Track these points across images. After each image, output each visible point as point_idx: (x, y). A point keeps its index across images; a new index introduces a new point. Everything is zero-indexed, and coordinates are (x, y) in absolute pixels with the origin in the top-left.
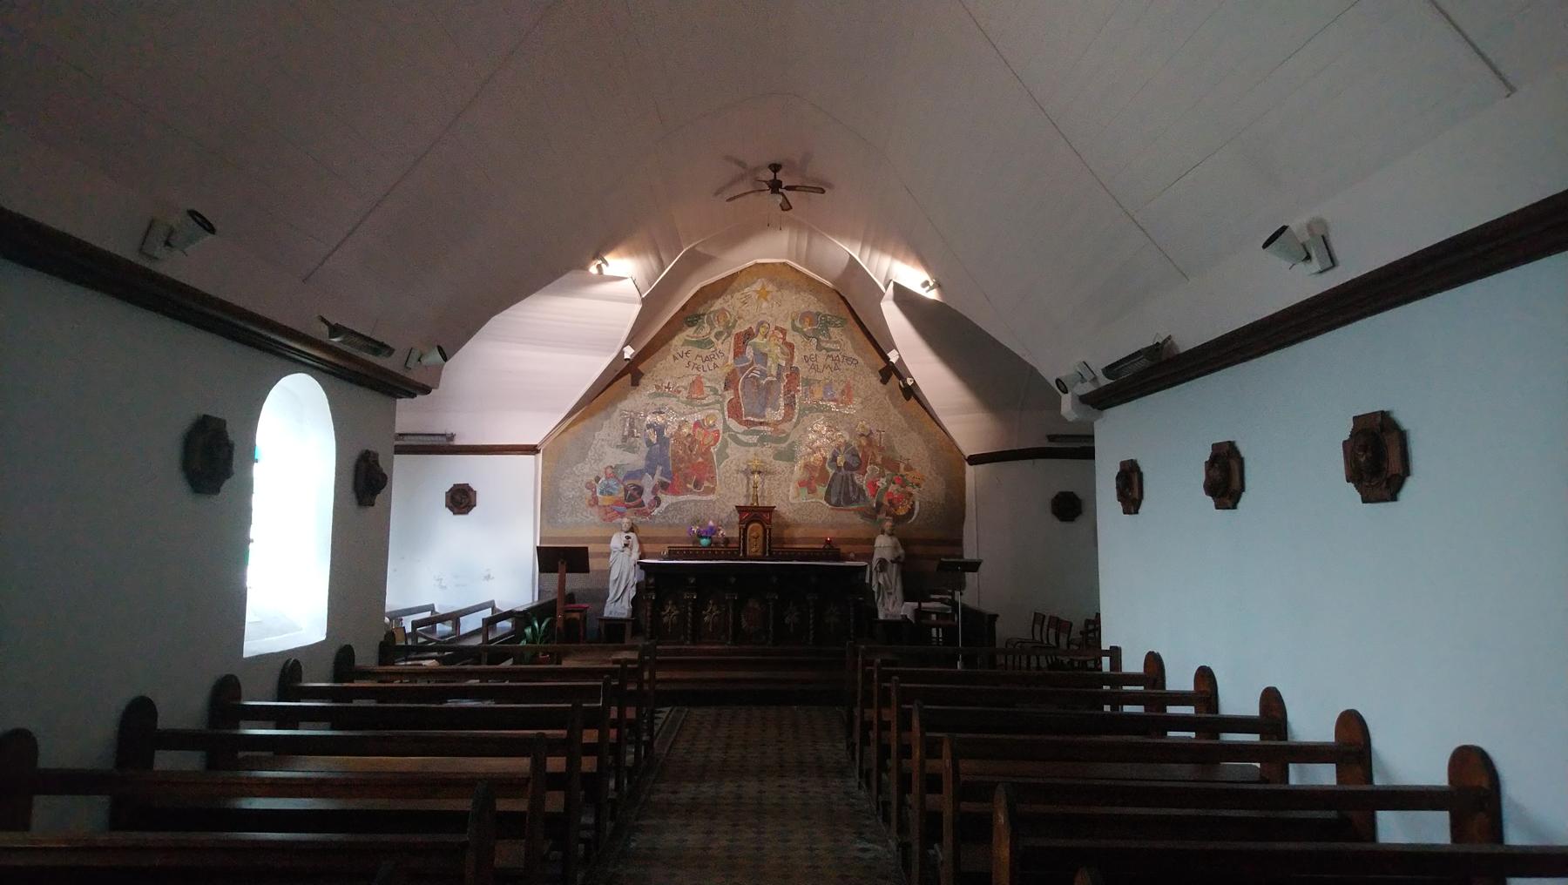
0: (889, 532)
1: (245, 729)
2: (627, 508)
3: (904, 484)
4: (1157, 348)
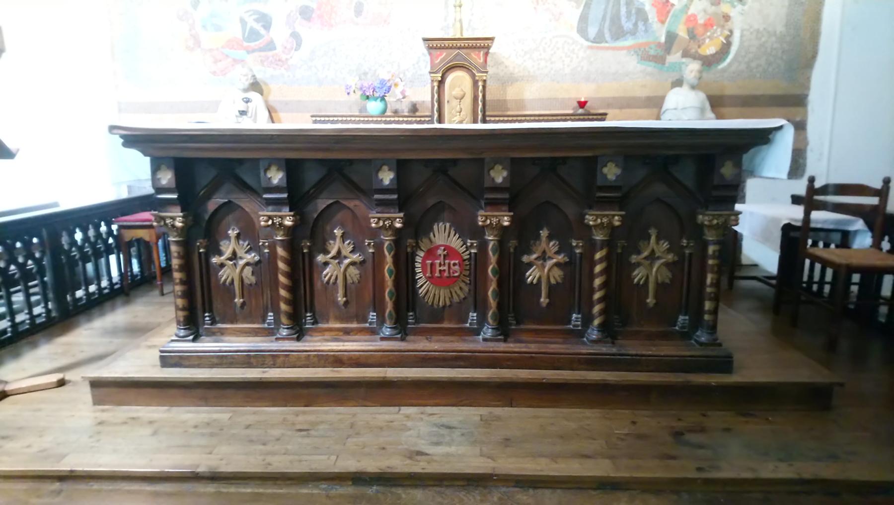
0: (695, 82)
2: (248, 52)
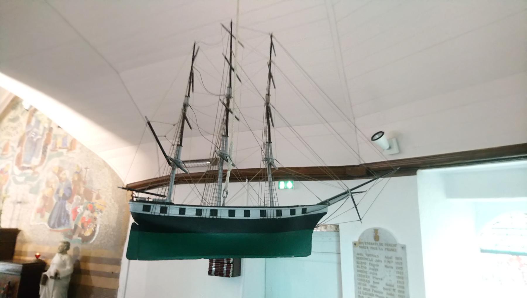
1: (13, 270)
3: (93, 211)
4: (219, 273)
